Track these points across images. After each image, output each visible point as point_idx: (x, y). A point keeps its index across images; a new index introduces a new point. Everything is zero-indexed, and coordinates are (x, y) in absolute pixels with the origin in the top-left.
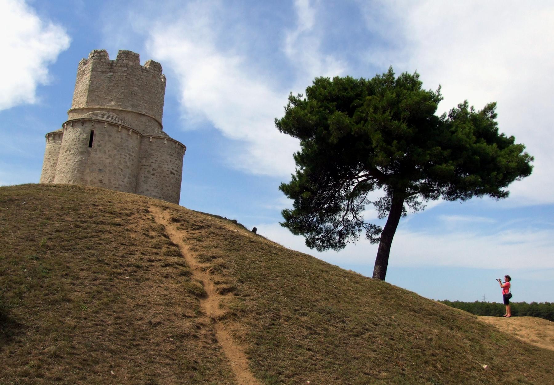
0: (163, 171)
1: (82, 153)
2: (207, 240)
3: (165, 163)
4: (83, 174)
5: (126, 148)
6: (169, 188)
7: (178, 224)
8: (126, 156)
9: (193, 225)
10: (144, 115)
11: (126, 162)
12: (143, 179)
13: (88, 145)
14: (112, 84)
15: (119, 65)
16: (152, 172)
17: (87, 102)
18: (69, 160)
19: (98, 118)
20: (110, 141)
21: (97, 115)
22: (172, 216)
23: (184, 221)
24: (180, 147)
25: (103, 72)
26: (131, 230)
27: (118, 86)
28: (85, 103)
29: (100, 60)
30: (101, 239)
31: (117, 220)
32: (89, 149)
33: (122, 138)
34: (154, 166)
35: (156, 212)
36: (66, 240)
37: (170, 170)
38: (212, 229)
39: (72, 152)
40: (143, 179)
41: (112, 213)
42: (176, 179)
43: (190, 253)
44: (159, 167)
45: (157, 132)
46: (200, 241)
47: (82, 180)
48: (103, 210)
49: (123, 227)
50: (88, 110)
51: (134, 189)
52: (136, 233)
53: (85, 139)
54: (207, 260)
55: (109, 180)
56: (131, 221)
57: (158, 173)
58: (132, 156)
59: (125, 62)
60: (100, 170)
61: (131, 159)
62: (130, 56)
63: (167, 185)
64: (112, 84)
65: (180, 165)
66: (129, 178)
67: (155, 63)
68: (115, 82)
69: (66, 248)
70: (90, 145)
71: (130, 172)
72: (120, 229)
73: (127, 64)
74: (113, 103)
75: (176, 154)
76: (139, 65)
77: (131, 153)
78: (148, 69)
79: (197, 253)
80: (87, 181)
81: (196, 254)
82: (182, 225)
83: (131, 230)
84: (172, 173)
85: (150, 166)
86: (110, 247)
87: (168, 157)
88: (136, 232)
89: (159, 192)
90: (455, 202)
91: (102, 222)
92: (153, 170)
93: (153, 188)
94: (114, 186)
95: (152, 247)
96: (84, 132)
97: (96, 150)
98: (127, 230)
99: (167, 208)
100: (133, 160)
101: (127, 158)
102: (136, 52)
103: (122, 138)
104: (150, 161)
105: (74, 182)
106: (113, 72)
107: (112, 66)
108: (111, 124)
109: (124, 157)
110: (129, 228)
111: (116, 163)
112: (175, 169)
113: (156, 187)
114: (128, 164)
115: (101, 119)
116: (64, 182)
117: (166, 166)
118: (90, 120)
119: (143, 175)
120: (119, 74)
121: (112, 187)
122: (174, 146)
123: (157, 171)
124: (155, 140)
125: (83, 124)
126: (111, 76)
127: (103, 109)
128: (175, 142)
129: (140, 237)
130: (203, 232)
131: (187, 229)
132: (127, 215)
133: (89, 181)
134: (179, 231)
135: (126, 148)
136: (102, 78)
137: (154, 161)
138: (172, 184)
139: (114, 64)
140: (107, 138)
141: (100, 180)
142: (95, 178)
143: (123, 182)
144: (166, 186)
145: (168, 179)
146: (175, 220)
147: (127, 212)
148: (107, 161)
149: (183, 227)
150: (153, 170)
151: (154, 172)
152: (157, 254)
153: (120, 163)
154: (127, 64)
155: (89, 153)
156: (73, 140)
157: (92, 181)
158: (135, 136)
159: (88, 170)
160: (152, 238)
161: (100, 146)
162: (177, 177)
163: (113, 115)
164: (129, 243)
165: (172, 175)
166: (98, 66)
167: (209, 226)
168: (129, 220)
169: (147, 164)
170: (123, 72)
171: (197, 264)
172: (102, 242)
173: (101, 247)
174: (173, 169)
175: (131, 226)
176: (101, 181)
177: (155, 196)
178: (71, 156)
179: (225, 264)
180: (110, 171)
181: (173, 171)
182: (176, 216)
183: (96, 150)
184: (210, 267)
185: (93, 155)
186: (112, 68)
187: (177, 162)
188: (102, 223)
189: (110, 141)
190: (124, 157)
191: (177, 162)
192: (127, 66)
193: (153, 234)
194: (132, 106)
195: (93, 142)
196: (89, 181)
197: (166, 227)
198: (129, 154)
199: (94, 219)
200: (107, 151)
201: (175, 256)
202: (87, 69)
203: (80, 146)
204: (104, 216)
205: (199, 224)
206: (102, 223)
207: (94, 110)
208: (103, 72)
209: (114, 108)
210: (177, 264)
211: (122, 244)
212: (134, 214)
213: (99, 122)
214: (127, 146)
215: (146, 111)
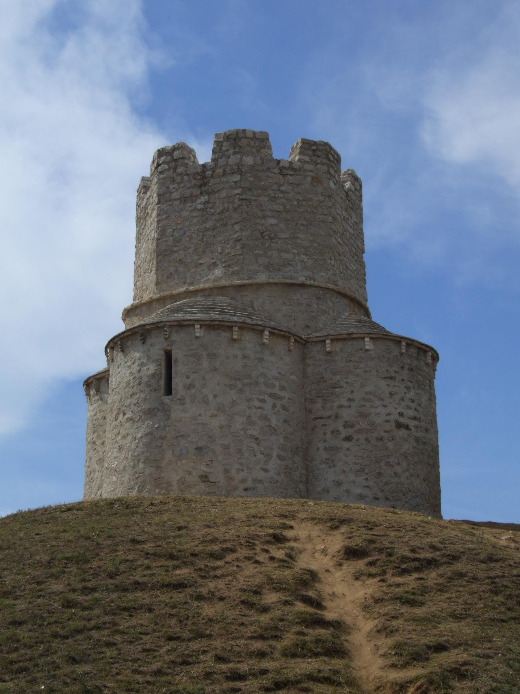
0: (373, 424)
1: (150, 413)
2: (438, 598)
3: (378, 403)
4: (158, 467)
5: (261, 380)
6: (399, 469)
7: (361, 564)
8: (263, 401)
9: (404, 559)
10: (302, 286)
11: (265, 418)
12: (324, 455)
13: (162, 391)
14: (209, 225)
15: (220, 171)
16: (344, 433)
17: (157, 283)
18: (124, 437)
19: (180, 316)
20: (215, 370)
21: (177, 310)
22: (348, 543)
23: (380, 551)
24: (413, 351)
25: (184, 200)
26: (211, 597)
27: (225, 225)
28: (153, 287)
29: (175, 168)
30: (117, 632)
31: (182, 573)
32: (167, 399)
33: (244, 357)
34: (346, 414)
35: (310, 538)
36: (25, 646)
37: (392, 418)
38: (460, 566)
39: (129, 415)
40: (324, 455)
41: (172, 557)
42: (417, 440)
43: (372, 644)
44: (363, 415)
45: (348, 321)
46: (412, 603)
47: (158, 482)
48: (151, 551)
49: (189, 590)
50: (162, 300)
51: (302, 486)
52: (221, 604)
53: (153, 375)
54: (417, 657)
55: (226, 471)
56: (218, 572)
57: (360, 431)
58: (281, 398)
59: (233, 160)
60: (199, 449)
61: (278, 407)
62: (243, 142)
63: (392, 460)
64: (209, 225)
65: (424, 399)
66: (279, 457)
67: (315, 143)
68: (216, 217)
69: (16, 666)
70: (169, 391)
71: (282, 441)
72: (179, 596)
73: (240, 165)
74: (218, 272)
75: (406, 372)
76: (272, 160)
77: (276, 391)
78: (297, 165)
79: (390, 641)
80: (169, 484)
81: (386, 643)
82: (371, 564)
83: (211, 597)
84: (399, 425)
85: (337, 417)
86: (133, 650)
87: (383, 384)
88: (221, 599)
89: (371, 483)
90: (367, 281)
91: (137, 583)
92: (346, 425)
93: (352, 477)
94: (242, 486)
95: (252, 638)
96: (149, 358)
97: (182, 401)
98: (199, 598)
99: (343, 522)
100: (284, 408)
101: (268, 406)
102: (257, 129)
103: (244, 357)
104: (335, 404)
105: (140, 491)
106: (209, 194)
107: (204, 177)
108: (211, 326)
109: (257, 404)
110: (204, 591)
111: (239, 422)
112: (411, 413)
113: (362, 470)
114: (274, 421)
115: (188, 317)
116: (119, 494)
117: (381, 409)
118: (157, 326)
119: (321, 445)
120: (224, 194)
121: (236, 489)
122: (396, 352)
123: (357, 427)
124: (338, 346)
125: (144, 341)
126: (205, 203)
127: (195, 293)
128: (398, 340)
129: (228, 613)
130: (432, 577)
131: (384, 572)
132: (213, 556)
133: (175, 483)
134: (358, 583)
135: (261, 380)
136: (185, 214)
137: (346, 403)
138: (405, 456)
139: (209, 173)
140: (205, 363)
141: (201, 477)
142: (190, 473)
143: (266, 470)
144: (388, 464)
145: (391, 445)
146: (352, 553)
147: (216, 548)
148: (215, 423)
149: (373, 570)
150: (346, 425)
151: (350, 431)
152: (262, 655)
153: (250, 422)
154: (240, 165)
155: (166, 411)
156: (128, 383)
157: (182, 482)
158: (281, 346)
159: (169, 455)
160: (265, 610)
161: (190, 387)
162: (419, 434)
163: (222, 300)
164: (191, 631)
165: (403, 432)
166: (172, 187)
167: (454, 558)
168: (215, 568)
169: (328, 413)
170: (232, 188)
171: (381, 673)
172: (118, 638)
173: (109, 652)
174: (401, 414)
175: (212, 585)
176: (204, 478)
177: (361, 497)
178: (128, 425)
179: (465, 664)
180: (226, 447)
181: (401, 420)
182: (358, 541)
183: (182, 401)
184: (417, 678)
185: (176, 413)
186: (205, 184)
187: (411, 394)
188: (138, 586)
189: (215, 370)
190: (257, 404)
191: (411, 394)
192: (239, 170)
193: (271, 598)
194: (268, 267)
195: (174, 381)
196: (175, 483)
197: (322, 575)
198: (272, 395)
199: (118, 580)
200: (211, 397)
201: (316, 655)
202: (151, 200)
203: (143, 396)
204: (148, 568)
205: (423, 555)
206: (138, 586)
207: (174, 298)
208: (184, 200)
209: (223, 283)
210: (311, 677)
211: (170, 639)
212: (233, 551)
213: (181, 325)
214: (263, 375)
215: (307, 273)
